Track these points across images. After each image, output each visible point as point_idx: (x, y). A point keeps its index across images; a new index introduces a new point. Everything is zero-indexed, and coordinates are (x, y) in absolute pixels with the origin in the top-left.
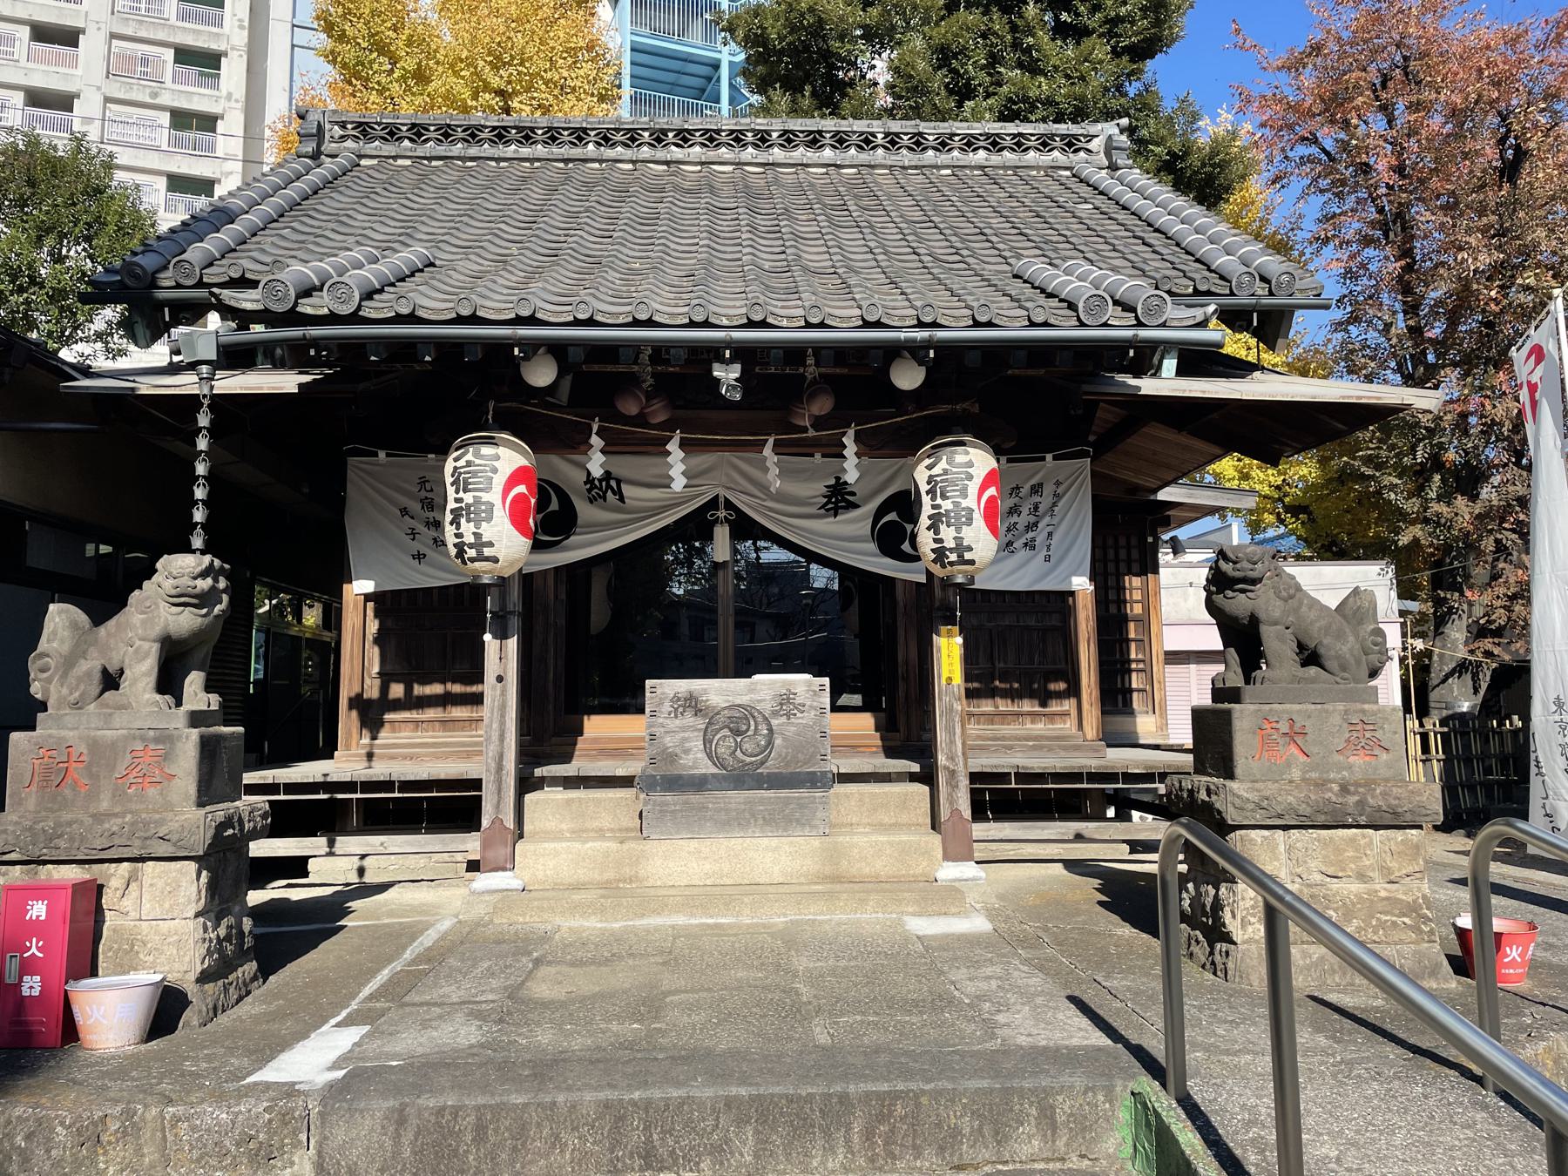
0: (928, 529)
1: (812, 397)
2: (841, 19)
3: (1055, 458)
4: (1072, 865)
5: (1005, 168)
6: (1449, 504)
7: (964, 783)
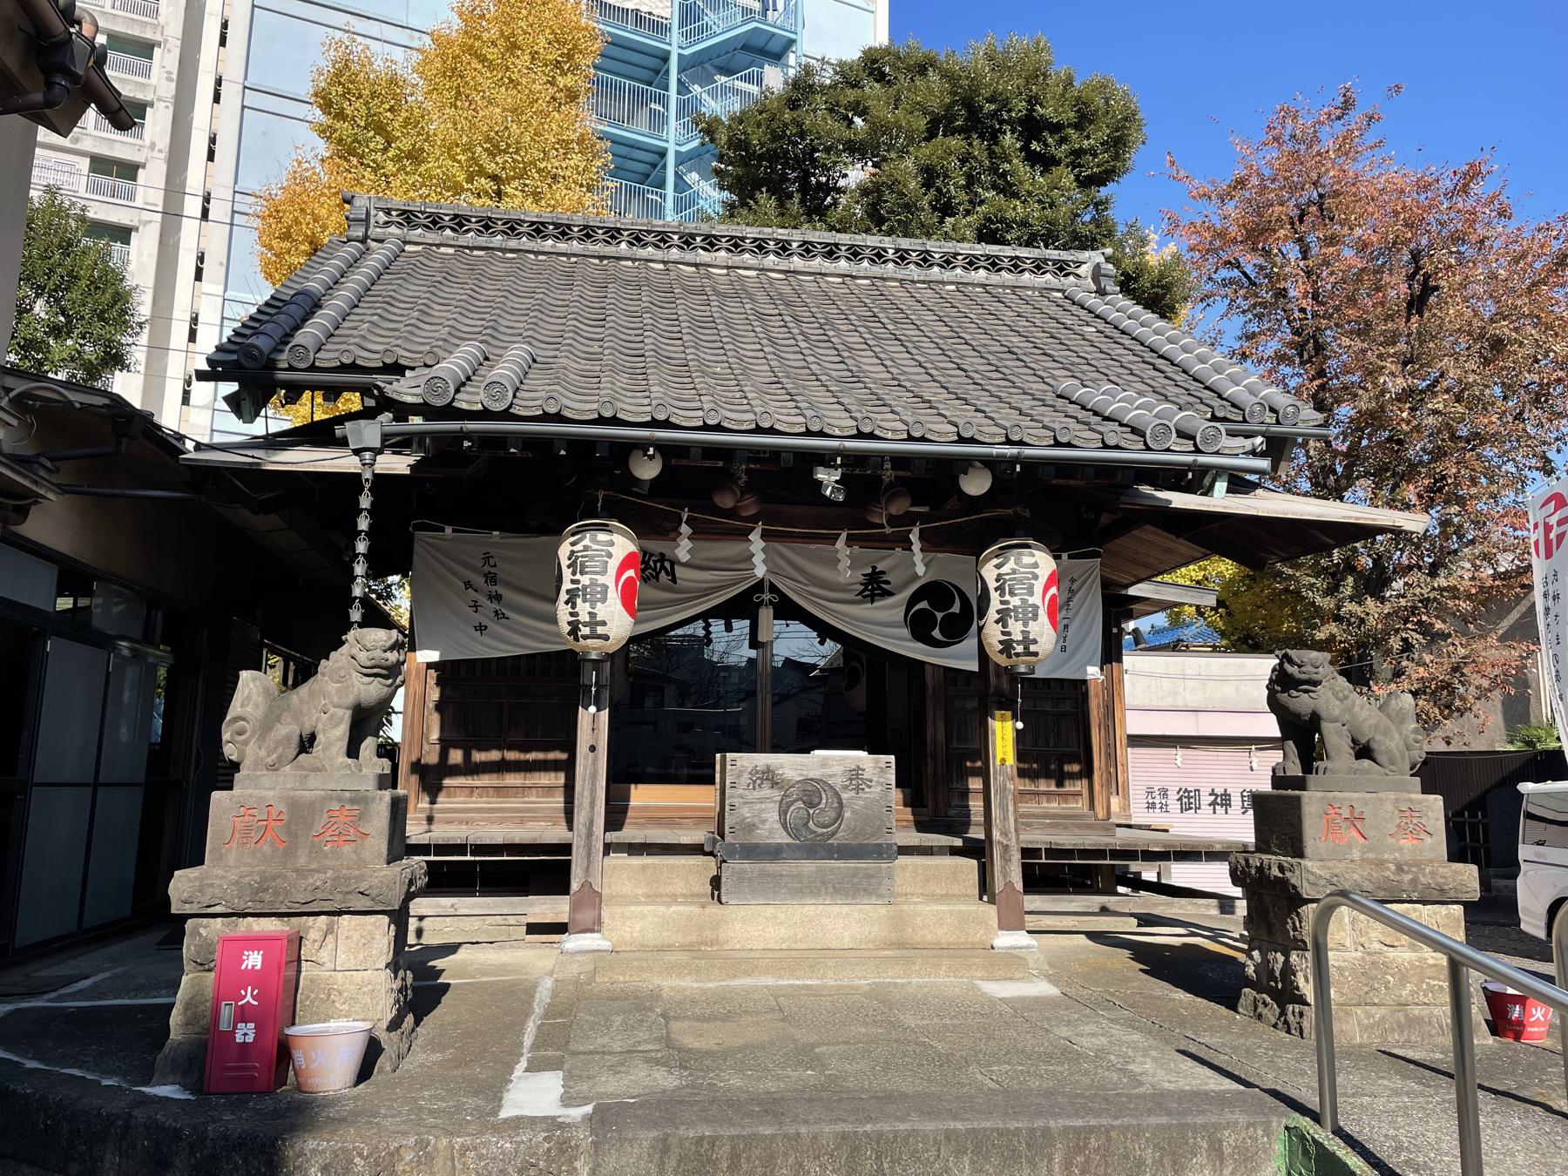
0: (997, 622)
1: (891, 499)
2: (829, 133)
3: (1070, 557)
4: (1093, 936)
5: (1004, 287)
6: (1360, 603)
7: (1016, 857)
